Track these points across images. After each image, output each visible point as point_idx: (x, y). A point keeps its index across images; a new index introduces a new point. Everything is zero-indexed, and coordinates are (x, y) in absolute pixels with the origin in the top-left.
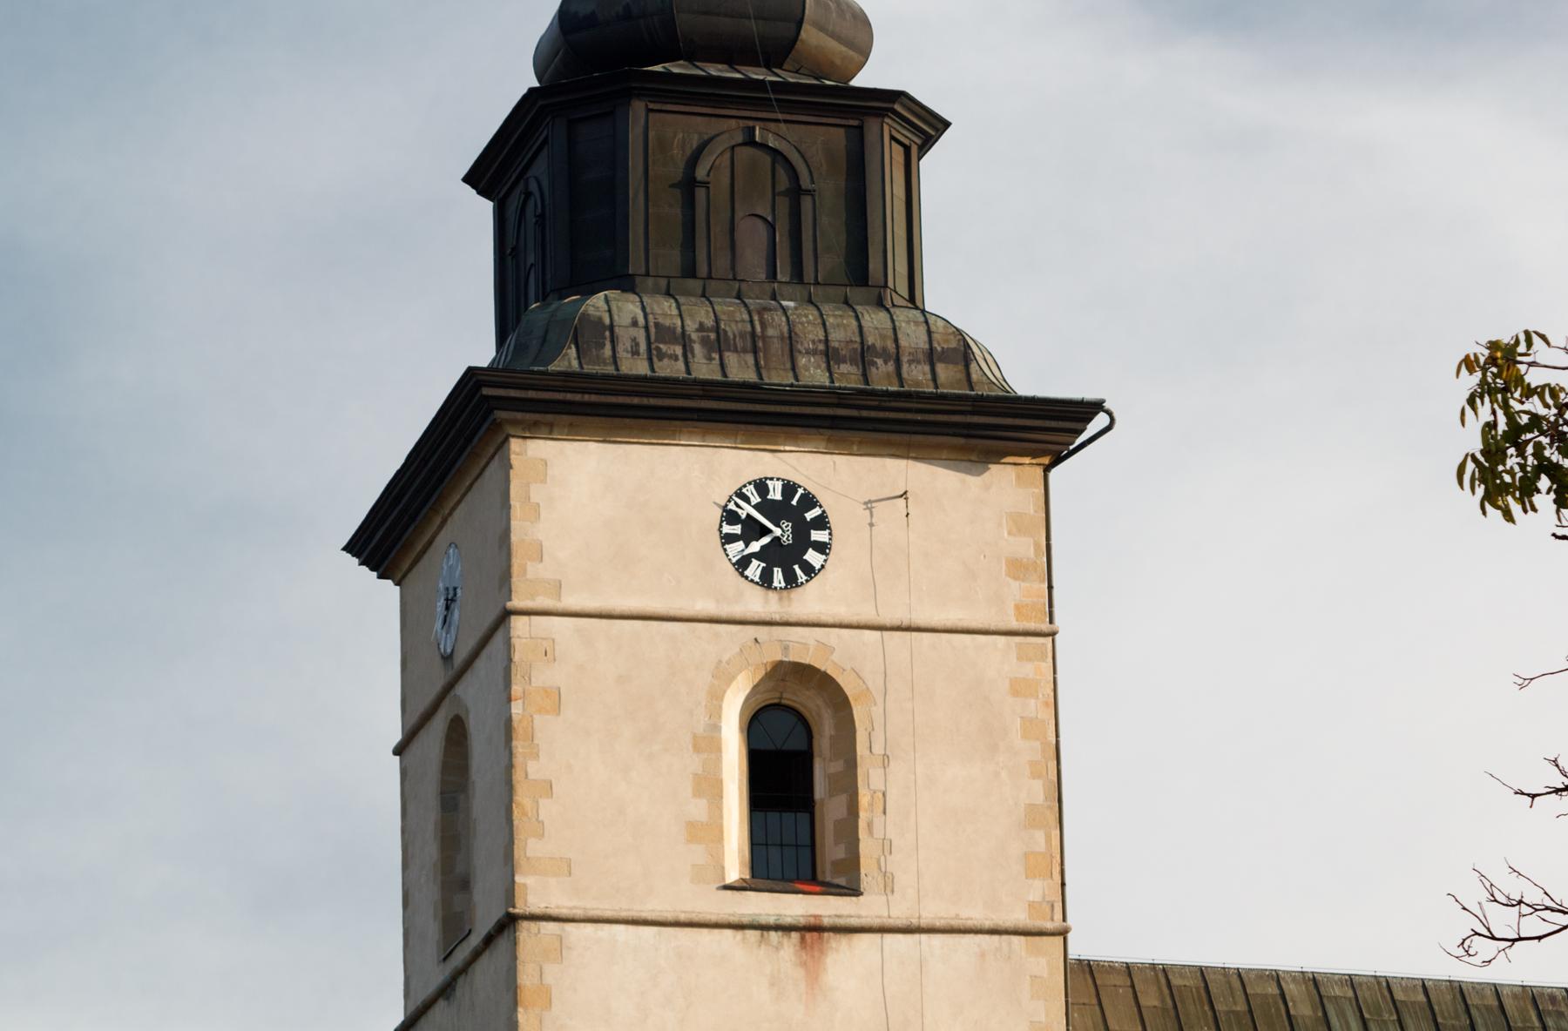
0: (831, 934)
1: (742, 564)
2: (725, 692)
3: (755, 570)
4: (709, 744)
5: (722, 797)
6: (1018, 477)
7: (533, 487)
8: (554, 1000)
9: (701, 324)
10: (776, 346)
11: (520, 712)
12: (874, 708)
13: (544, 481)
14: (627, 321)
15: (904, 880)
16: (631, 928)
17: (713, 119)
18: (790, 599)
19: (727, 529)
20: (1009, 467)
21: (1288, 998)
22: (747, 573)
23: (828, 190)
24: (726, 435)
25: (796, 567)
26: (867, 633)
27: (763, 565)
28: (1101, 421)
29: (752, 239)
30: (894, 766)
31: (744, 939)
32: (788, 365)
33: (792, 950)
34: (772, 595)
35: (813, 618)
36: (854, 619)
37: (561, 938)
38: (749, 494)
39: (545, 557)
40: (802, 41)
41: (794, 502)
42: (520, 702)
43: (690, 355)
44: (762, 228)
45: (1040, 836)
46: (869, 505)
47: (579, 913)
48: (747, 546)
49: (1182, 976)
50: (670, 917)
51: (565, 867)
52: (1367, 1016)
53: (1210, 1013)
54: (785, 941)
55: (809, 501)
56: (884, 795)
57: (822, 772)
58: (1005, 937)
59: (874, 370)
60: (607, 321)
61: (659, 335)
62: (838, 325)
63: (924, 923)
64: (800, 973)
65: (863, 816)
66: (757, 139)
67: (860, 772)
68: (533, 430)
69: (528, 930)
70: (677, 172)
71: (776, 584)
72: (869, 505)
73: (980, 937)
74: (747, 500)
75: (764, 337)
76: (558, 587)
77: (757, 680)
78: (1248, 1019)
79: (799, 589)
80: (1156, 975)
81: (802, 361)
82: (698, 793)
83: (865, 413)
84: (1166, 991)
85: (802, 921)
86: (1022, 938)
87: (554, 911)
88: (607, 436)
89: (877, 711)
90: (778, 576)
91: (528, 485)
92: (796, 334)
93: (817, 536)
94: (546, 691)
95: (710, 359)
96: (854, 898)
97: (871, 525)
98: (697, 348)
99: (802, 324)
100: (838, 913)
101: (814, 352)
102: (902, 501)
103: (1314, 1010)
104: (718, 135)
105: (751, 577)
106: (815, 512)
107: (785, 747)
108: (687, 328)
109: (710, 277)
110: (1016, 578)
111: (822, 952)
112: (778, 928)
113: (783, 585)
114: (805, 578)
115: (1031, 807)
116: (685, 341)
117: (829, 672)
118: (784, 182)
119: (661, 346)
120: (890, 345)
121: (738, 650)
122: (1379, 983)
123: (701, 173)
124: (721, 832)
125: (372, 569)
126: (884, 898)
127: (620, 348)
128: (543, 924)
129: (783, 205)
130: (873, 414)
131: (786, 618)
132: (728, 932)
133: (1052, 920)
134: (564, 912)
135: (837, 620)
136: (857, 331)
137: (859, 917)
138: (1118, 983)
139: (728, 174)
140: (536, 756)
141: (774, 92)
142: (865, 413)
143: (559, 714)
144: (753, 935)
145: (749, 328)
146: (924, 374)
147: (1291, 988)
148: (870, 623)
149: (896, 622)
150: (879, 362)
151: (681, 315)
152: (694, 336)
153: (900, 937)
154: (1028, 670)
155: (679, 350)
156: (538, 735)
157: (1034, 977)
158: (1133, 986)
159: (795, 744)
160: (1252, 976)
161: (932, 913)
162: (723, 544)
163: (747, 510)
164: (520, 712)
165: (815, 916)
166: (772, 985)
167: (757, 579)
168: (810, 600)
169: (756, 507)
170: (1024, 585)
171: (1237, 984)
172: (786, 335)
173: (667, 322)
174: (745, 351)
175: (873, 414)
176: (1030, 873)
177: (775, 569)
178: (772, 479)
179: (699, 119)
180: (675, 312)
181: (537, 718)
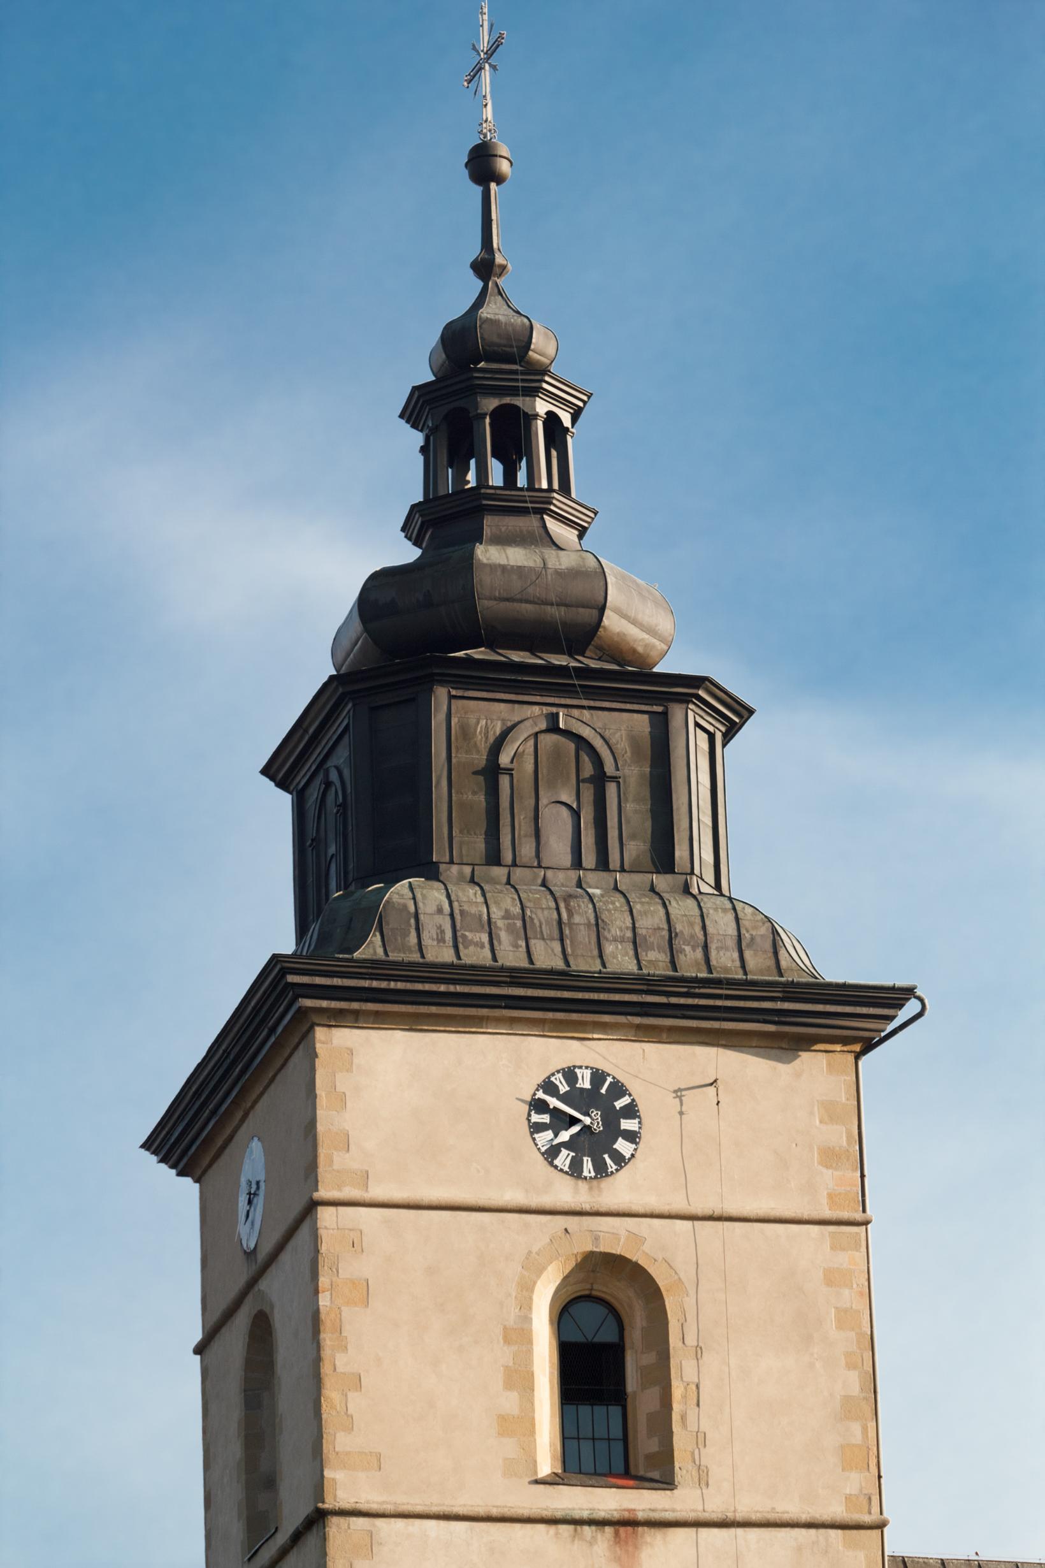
1: (552, 1153)
2: (535, 1283)
3: (564, 1158)
4: (519, 1336)
6: (829, 1065)
7: (339, 1076)
9: (507, 911)
11: (328, 1304)
12: (686, 1299)
13: (349, 1070)
15: (717, 1473)
16: (443, 1524)
17: (516, 706)
18: (600, 1190)
19: (536, 1118)
22: (557, 1162)
25: (606, 1156)
26: (679, 1223)
28: (911, 1008)
30: (707, 1357)
31: (557, 1534)
33: (606, 1545)
39: (352, 1147)
40: (600, 638)
42: (328, 1294)
43: (495, 942)
45: (856, 1428)
46: (678, 1093)
47: (389, 1508)
48: (556, 1135)
50: (481, 1511)
54: (599, 1536)
55: (618, 1089)
58: (822, 1531)
59: (682, 957)
63: (739, 1517)
65: (676, 1407)
68: (338, 1019)
69: (338, 1526)
70: (480, 759)
71: (586, 1173)
72: (678, 1093)
76: (365, 1178)
77: (567, 1272)
79: (610, 1179)
82: (509, 1385)
85: (616, 1516)
86: (840, 1532)
87: (363, 1507)
88: (413, 1023)
89: (689, 1302)
92: (603, 921)
93: (627, 1124)
95: (517, 946)
96: (668, 1492)
99: (609, 911)
100: (652, 1507)
101: (622, 940)
102: (712, 1089)
108: (493, 916)
109: (515, 864)
110: (827, 1167)
111: (636, 1547)
112: (591, 1522)
113: (593, 1174)
114: (615, 1167)
115: (847, 1400)
118: (588, 770)
123: (504, 759)
124: (533, 1425)
127: (425, 936)
130: (682, 1001)
131: (596, 1208)
132: (541, 1527)
133: (870, 1513)
134: (374, 1507)
136: (664, 918)
137: (673, 1511)
145: (555, 915)
149: (708, 1212)
152: (500, 923)
153: (715, 1531)
155: (485, 938)
159: (607, 1336)
161: (747, 1506)
162: (532, 1134)
165: (629, 1511)
167: (566, 1169)
170: (837, 1173)
175: (682, 1001)
176: (847, 1466)
178: (580, 1067)
179: (502, 705)
180: (480, 899)
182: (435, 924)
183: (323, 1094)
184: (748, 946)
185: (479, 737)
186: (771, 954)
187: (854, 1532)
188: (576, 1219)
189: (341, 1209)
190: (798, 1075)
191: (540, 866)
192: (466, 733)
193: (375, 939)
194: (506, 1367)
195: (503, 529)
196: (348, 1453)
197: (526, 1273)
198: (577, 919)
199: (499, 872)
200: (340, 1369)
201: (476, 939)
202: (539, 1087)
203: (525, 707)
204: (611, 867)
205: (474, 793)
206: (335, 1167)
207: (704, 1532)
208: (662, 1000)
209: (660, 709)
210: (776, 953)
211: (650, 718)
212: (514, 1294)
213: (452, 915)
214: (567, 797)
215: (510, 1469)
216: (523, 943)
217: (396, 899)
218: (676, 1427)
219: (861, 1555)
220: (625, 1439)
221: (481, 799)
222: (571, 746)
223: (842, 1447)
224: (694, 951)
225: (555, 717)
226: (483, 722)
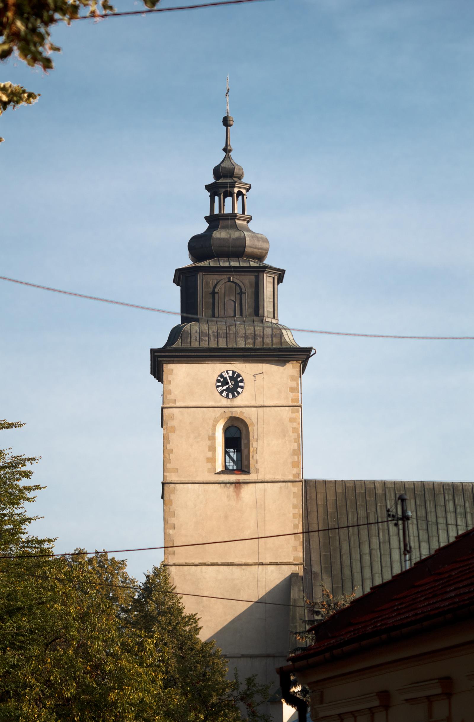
0: (243, 484)
1: (221, 393)
2: (216, 425)
3: (225, 394)
4: (212, 438)
5: (215, 451)
6: (293, 366)
7: (169, 376)
8: (173, 503)
9: (213, 331)
10: (232, 336)
11: (165, 432)
12: (254, 427)
13: (172, 374)
14: (194, 331)
15: (261, 470)
16: (192, 485)
17: (220, 276)
18: (233, 401)
19: (218, 384)
20: (290, 364)
21: (376, 488)
22: (223, 395)
23: (249, 291)
24: (218, 360)
25: (235, 393)
26: (253, 408)
27: (227, 392)
28: (313, 352)
29: (230, 306)
30: (259, 441)
31: (221, 486)
32: (235, 341)
33: (233, 488)
34: (229, 400)
35: (239, 405)
36: (249, 405)
37: (175, 488)
38: (229, 373)
39: (172, 394)
40: (246, 251)
41: (235, 376)
42: (165, 430)
43: (210, 340)
44: (232, 303)
45: (296, 457)
46: (254, 376)
47: (179, 482)
48: (222, 387)
49: (349, 483)
50: (201, 481)
51: (176, 470)
52: (396, 492)
53: (354, 493)
54: (231, 486)
55: (239, 375)
56: (256, 449)
57: (243, 442)
58: (287, 483)
59: (257, 340)
60: (189, 332)
61: (201, 334)
62: (249, 329)
63: (265, 480)
64: (234, 494)
65: (251, 454)
66: (231, 280)
67: (250, 443)
68: (169, 362)
69: (167, 486)
70: (211, 290)
71: (230, 397)
72: (254, 376)
73: (280, 483)
74: (228, 374)
75: (229, 334)
76: (175, 401)
77: (226, 421)
78: (364, 495)
79: (236, 398)
80: (343, 483)
81: (238, 339)
82: (209, 450)
83: (252, 354)
84: (344, 487)
85: (235, 481)
86: (291, 483)
87: (172, 482)
88: (187, 362)
89: (255, 428)
90: (230, 395)
91: (168, 375)
92: (237, 332)
93: (241, 384)
94: (172, 427)
95: (215, 340)
96: (248, 475)
97: (255, 381)
98: (212, 338)
99: (239, 329)
100: (244, 479)
101: (242, 337)
102: (262, 374)
103: (383, 491)
104: (221, 280)
105: (224, 396)
106: (240, 378)
107: (235, 436)
108: (209, 333)
109: (218, 317)
110: (291, 392)
111: (240, 489)
112: (229, 483)
113: (232, 397)
114: (237, 395)
115: (294, 450)
116: (209, 336)
117: (243, 419)
118: (238, 291)
119: (203, 338)
120: (261, 333)
121: (220, 414)
122: (402, 483)
123: (216, 290)
124: (215, 460)
125: (157, 380)
126: (256, 475)
127: (192, 339)
128: (170, 485)
129: (238, 297)
130: (253, 354)
131: (232, 406)
132: (217, 485)
133: (299, 478)
134: (175, 481)
135: (245, 405)
136: (253, 331)
137: (250, 479)
138: (332, 486)
139: (224, 290)
140: (169, 443)
141: (233, 268)
142: (252, 354)
143: (175, 432)
144: (223, 485)
145: (225, 331)
146: (270, 341)
147: (377, 485)
148: (253, 406)
149: (260, 405)
150: (258, 338)
151: (208, 329)
152: (211, 335)
153: (260, 484)
154: (294, 415)
155: (207, 339)
156: (170, 438)
157: (294, 493)
158: (336, 487)
159: (237, 435)
160: (368, 482)
161: (268, 477)
162: (217, 388)
163: (226, 375)
164: (165, 432)
165: (238, 480)
166: (227, 497)
167: (225, 396)
168: (239, 401)
169: (229, 376)
170: (294, 394)
171: (363, 485)
172: (235, 332)
173: (205, 331)
174: (224, 338)
175: (253, 354)
176: (293, 467)
177: (230, 393)
178: (229, 371)
179: (217, 276)
180: (207, 328)
181: (169, 433)
182: (195, 335)
183: (165, 381)
184: (274, 337)
185: (211, 285)
186: (280, 338)
187: (295, 483)
188: (227, 409)
189: (169, 409)
190: (284, 369)
191: (225, 317)
192: (207, 283)
193: (179, 340)
194: (209, 446)
195: (225, 224)
196: (169, 468)
197: (214, 423)
198: (231, 332)
199: (214, 319)
200: (168, 448)
201: (205, 339)
202: (219, 376)
203: (223, 276)
204: (243, 316)
205: (209, 299)
206: (168, 399)
207: (257, 484)
208: (249, 354)
209: (257, 274)
210: (281, 338)
211: (255, 277)
212: (211, 428)
213: (199, 333)
214: (233, 298)
215: (209, 471)
216: (216, 339)
217: (186, 329)
218: (251, 459)
219: (296, 489)
220: (241, 461)
221: (211, 300)
222: (234, 285)
223: (292, 462)
224: (260, 338)
225: (230, 278)
226: (212, 281)
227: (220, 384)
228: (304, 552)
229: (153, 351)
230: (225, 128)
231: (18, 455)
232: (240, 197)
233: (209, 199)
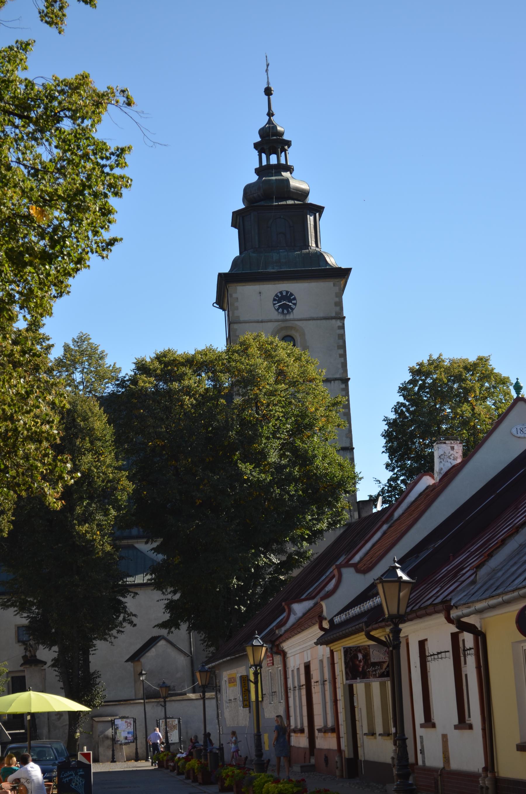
106: (293, 297)
227: (276, 302)
228: (367, 538)
229: (220, 275)
230: (267, 97)
231: (48, 26)
232: (283, 153)
233: (258, 157)
